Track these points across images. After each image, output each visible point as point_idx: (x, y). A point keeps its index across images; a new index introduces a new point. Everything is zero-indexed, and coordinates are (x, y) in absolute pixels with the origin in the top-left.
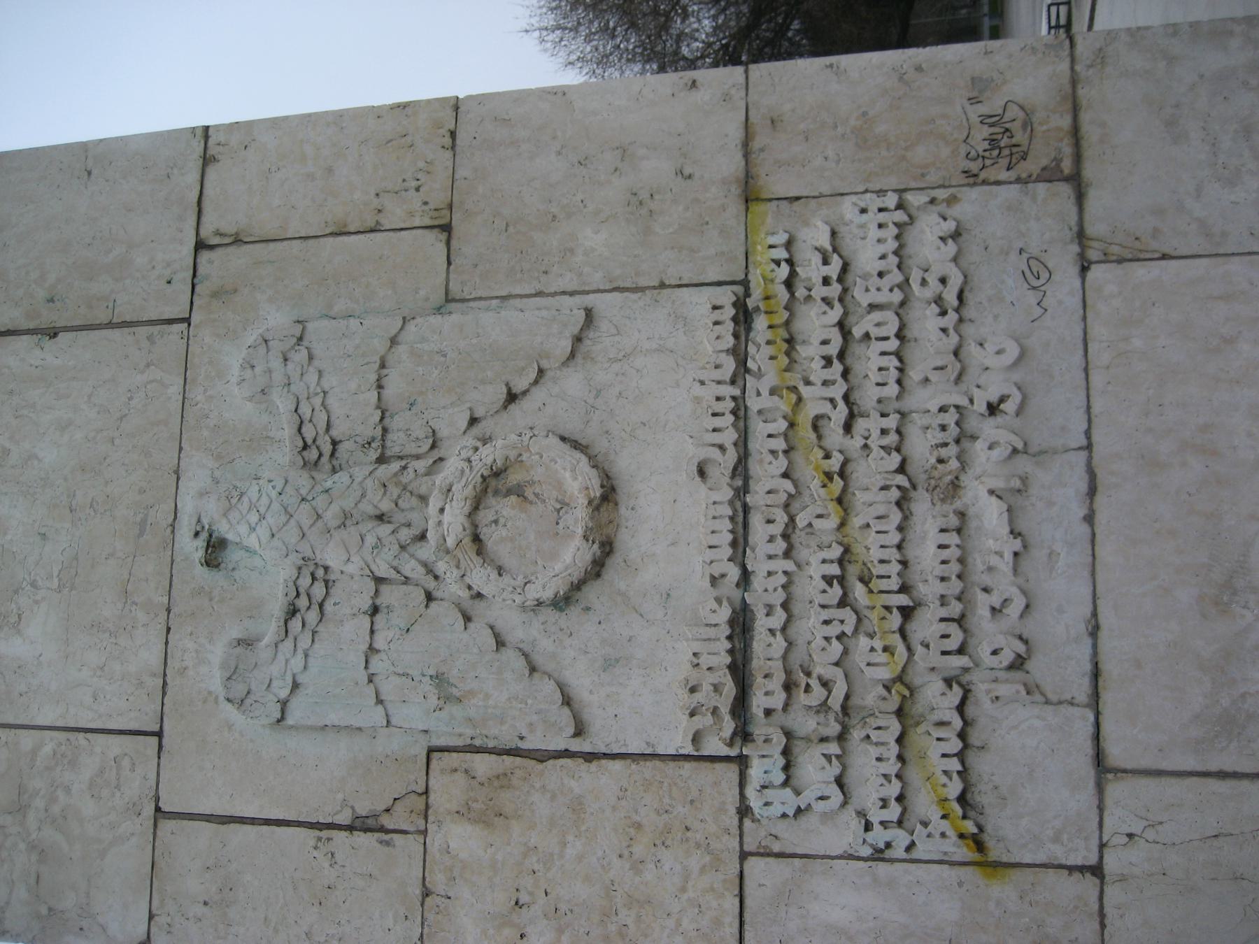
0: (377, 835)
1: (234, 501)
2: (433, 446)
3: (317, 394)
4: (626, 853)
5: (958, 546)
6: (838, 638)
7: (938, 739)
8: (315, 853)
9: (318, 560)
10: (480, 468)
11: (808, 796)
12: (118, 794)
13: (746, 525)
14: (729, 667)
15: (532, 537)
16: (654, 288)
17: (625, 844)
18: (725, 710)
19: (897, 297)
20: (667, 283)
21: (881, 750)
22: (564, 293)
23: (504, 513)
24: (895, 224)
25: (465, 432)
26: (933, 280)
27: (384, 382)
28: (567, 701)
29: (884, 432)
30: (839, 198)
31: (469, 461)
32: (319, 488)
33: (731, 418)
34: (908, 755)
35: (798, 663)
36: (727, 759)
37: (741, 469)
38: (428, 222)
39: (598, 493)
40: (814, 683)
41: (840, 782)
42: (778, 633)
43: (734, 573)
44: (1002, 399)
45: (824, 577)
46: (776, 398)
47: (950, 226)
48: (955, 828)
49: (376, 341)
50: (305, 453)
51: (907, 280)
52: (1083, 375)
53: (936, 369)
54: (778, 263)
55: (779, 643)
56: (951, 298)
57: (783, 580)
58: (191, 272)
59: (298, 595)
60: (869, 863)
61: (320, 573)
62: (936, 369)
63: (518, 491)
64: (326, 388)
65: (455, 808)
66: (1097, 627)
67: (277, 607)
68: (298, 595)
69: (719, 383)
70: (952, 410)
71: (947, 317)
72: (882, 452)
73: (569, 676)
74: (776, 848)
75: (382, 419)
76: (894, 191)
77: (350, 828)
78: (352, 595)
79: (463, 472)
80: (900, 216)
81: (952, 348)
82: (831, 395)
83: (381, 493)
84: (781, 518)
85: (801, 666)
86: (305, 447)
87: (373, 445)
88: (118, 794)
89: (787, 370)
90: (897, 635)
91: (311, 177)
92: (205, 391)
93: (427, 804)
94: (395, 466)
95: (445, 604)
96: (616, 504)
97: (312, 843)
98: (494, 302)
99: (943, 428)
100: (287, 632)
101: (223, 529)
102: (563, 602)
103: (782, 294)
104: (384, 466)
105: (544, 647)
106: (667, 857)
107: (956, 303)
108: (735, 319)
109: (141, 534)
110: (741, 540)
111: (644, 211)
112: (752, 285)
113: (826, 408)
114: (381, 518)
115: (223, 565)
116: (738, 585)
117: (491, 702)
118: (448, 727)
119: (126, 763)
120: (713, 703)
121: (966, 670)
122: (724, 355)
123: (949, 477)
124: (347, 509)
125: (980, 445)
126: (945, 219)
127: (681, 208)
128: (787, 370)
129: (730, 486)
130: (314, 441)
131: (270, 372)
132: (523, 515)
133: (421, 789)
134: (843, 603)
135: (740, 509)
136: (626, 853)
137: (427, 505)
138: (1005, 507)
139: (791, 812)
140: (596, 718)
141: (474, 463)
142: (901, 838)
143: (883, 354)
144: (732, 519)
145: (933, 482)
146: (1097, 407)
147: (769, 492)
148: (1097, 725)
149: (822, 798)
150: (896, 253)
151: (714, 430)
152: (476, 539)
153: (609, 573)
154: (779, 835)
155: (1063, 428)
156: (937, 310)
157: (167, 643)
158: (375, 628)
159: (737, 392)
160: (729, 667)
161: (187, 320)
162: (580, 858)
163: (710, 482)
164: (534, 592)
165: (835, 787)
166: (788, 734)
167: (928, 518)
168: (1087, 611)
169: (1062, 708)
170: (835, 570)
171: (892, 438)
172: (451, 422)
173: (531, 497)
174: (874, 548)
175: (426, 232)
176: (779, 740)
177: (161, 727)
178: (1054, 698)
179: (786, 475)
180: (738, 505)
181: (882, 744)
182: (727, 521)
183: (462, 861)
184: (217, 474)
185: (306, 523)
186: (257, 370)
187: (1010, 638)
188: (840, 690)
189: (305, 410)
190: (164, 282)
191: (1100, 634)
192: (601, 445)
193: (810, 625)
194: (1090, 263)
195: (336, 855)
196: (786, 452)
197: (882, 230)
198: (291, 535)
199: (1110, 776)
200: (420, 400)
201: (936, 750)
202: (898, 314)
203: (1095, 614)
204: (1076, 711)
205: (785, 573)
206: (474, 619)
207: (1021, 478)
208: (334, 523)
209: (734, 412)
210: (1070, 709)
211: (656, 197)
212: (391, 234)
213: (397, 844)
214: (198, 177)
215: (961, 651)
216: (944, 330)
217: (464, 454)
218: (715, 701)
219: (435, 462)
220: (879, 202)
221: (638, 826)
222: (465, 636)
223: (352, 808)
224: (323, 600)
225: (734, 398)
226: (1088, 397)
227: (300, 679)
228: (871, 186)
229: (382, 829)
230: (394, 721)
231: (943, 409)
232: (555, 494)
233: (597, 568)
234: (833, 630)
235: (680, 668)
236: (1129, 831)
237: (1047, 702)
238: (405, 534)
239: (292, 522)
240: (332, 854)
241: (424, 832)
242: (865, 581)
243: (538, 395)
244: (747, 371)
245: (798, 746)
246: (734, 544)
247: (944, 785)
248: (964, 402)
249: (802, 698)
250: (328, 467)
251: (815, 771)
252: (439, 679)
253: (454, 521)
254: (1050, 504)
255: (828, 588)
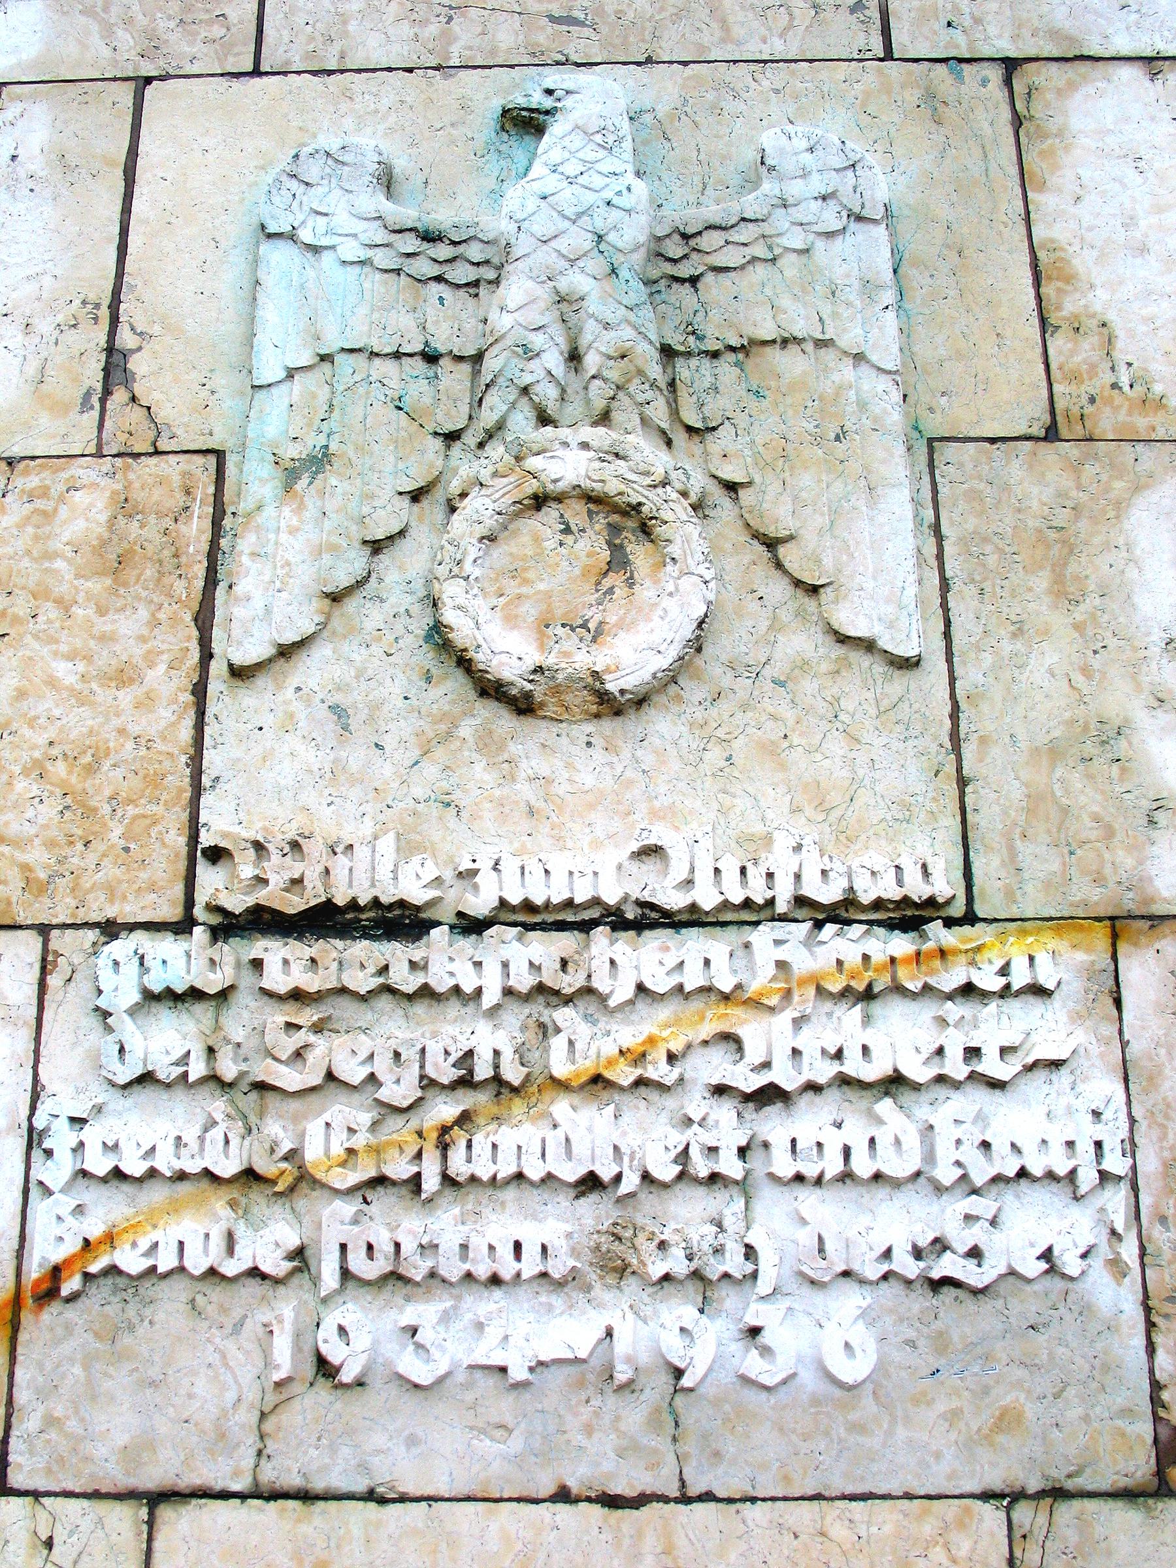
0: (99, 387)
1: (598, 138)
2: (690, 429)
3: (770, 248)
4: (55, 751)
5: (518, 1275)
6: (372, 1077)
7: (207, 1235)
8: (77, 303)
9: (507, 268)
10: (651, 501)
11: (127, 1029)
12: (172, 24)
13: (561, 926)
14: (329, 901)
15: (542, 586)
16: (959, 769)
17: (67, 748)
18: (262, 896)
19: (946, 1174)
20: (968, 789)
21: (194, 1145)
22: (948, 623)
23: (581, 544)
24: (1073, 1172)
25: (714, 476)
26: (977, 1235)
27: (793, 349)
28: (286, 652)
29: (713, 1150)
30: (1122, 1075)
31: (664, 484)
32: (618, 259)
33: (737, 899)
34: (184, 1188)
35: (336, 1013)
36: (189, 903)
37: (648, 919)
38: (1060, 405)
39: (612, 687)
40: (302, 1037)
41: (146, 1078)
42: (381, 980)
43: (480, 904)
44: (766, 1351)
45: (470, 1054)
46: (771, 970)
47: (1071, 1264)
48: (68, 1262)
49: (859, 331)
50: (676, 237)
51: (975, 1191)
52: (811, 1492)
53: (820, 1239)
54: (1004, 971)
55: (363, 982)
56: (948, 1266)
57: (468, 988)
58: (968, 56)
59: (454, 243)
60: (25, 1125)
61: (491, 275)
62: (820, 1239)
63: (618, 561)
64: (779, 263)
65: (133, 495)
66: (383, 1501)
67: (442, 217)
68: (454, 243)
69: (798, 877)
70: (749, 1268)
71: (911, 1260)
72: (680, 1148)
73: (321, 652)
74: (53, 981)
75: (733, 349)
76: (1134, 1168)
77: (110, 349)
78: (449, 322)
79: (647, 474)
80: (1087, 1178)
81: (856, 1267)
82: (775, 1064)
83: (612, 352)
84: (569, 983)
85: (329, 1017)
86: (685, 237)
87: (691, 339)
88: (172, 24)
89: (820, 991)
90: (373, 1173)
91: (1130, 222)
92: (777, 92)
93: (139, 455)
94: (655, 371)
95: (439, 463)
96: (597, 716)
97: (92, 297)
98: (929, 514)
99: (718, 1251)
100: (400, 231)
101: (557, 129)
102: (439, 637)
103: (951, 979)
104: (656, 355)
105: (366, 614)
106: (49, 812)
107: (936, 1274)
108: (906, 901)
109: (553, 19)
110: (537, 919)
111: (1090, 749)
112: (966, 929)
113: (754, 1054)
114: (574, 357)
115: (505, 136)
116: (460, 914)
117: (284, 537)
118: (254, 481)
119: (217, 31)
120: (273, 879)
121: (315, 1281)
122: (846, 885)
123: (635, 1261)
124: (585, 304)
125: (687, 1313)
126: (1084, 1256)
127: (1096, 809)
128: (820, 991)
129: (626, 898)
130: (694, 249)
131: (803, 176)
132: (577, 571)
133: (163, 445)
134: (428, 1083)
135: (587, 915)
136: (55, 751)
137: (595, 424)
138: (583, 1355)
139: (102, 1002)
140: (256, 700)
141: (660, 490)
142: (55, 1172)
143: (847, 1152)
144: (569, 904)
145: (628, 1234)
146: (756, 1513)
147: (612, 962)
148: (225, 1495)
149: (122, 1050)
150: (1023, 1173)
151: (717, 871)
152: (539, 501)
153: (487, 710)
154: (73, 984)
155: (717, 1454)
156: (923, 1242)
157: (390, 69)
158: (405, 360)
159: (781, 907)
160: (329, 901)
161: (888, 56)
162: (52, 682)
163: (633, 867)
164: (451, 592)
165: (139, 1072)
166: (224, 995)
167: (557, 1229)
168: (411, 1489)
169: (252, 1439)
170: (483, 1071)
171: (701, 1167)
172: (732, 455)
173: (607, 583)
174: (510, 1142)
175: (1045, 403)
176: (213, 983)
177: (267, 73)
178: (268, 1426)
179: (641, 988)
180: (594, 913)
181: (202, 1149)
182: (566, 895)
183: (56, 510)
184: (647, 118)
185: (561, 244)
186: (807, 158)
187: (365, 1356)
188: (289, 1078)
189: (745, 233)
190: (950, 17)
191: (372, 1505)
192: (693, 691)
193: (394, 1027)
194: (1008, 1509)
195: (73, 331)
196: (680, 988)
197: (1063, 1149)
198: (542, 225)
199: (144, 1513)
200: (765, 403)
201: (193, 1234)
202: (918, 1174)
203: (403, 1499)
204: (248, 1462)
205: (479, 991)
206: (416, 508)
207: (631, 1382)
208: (563, 284)
209: (747, 904)
210: (252, 1452)
211: (1115, 769)
212: (1039, 350)
213: (86, 415)
214: (1124, 52)
215: (346, 1274)
216: (887, 1254)
217: (674, 475)
218: (276, 881)
219: (664, 433)
220: (1113, 1147)
221: (91, 770)
222: (388, 492)
223: (140, 349)
224: (447, 281)
225: (771, 902)
226: (773, 1499)
227: (327, 258)
228: (1142, 1126)
229: (107, 392)
230: (261, 395)
231: (750, 1252)
232: (612, 619)
233: (491, 690)
234: (382, 1067)
235: (329, 820)
236: (55, 1541)
237: (263, 1415)
238: (547, 393)
239: (567, 224)
240: (74, 326)
241: (99, 454)
242: (464, 1118)
243: (777, 589)
244: (819, 925)
245: (203, 1011)
246: (528, 906)
247: (134, 1245)
248: (764, 1286)
249: (278, 1016)
250: (655, 274)
251: (167, 1040)
252: (320, 461)
253: (567, 464)
254: (589, 1430)
255: (452, 1059)
